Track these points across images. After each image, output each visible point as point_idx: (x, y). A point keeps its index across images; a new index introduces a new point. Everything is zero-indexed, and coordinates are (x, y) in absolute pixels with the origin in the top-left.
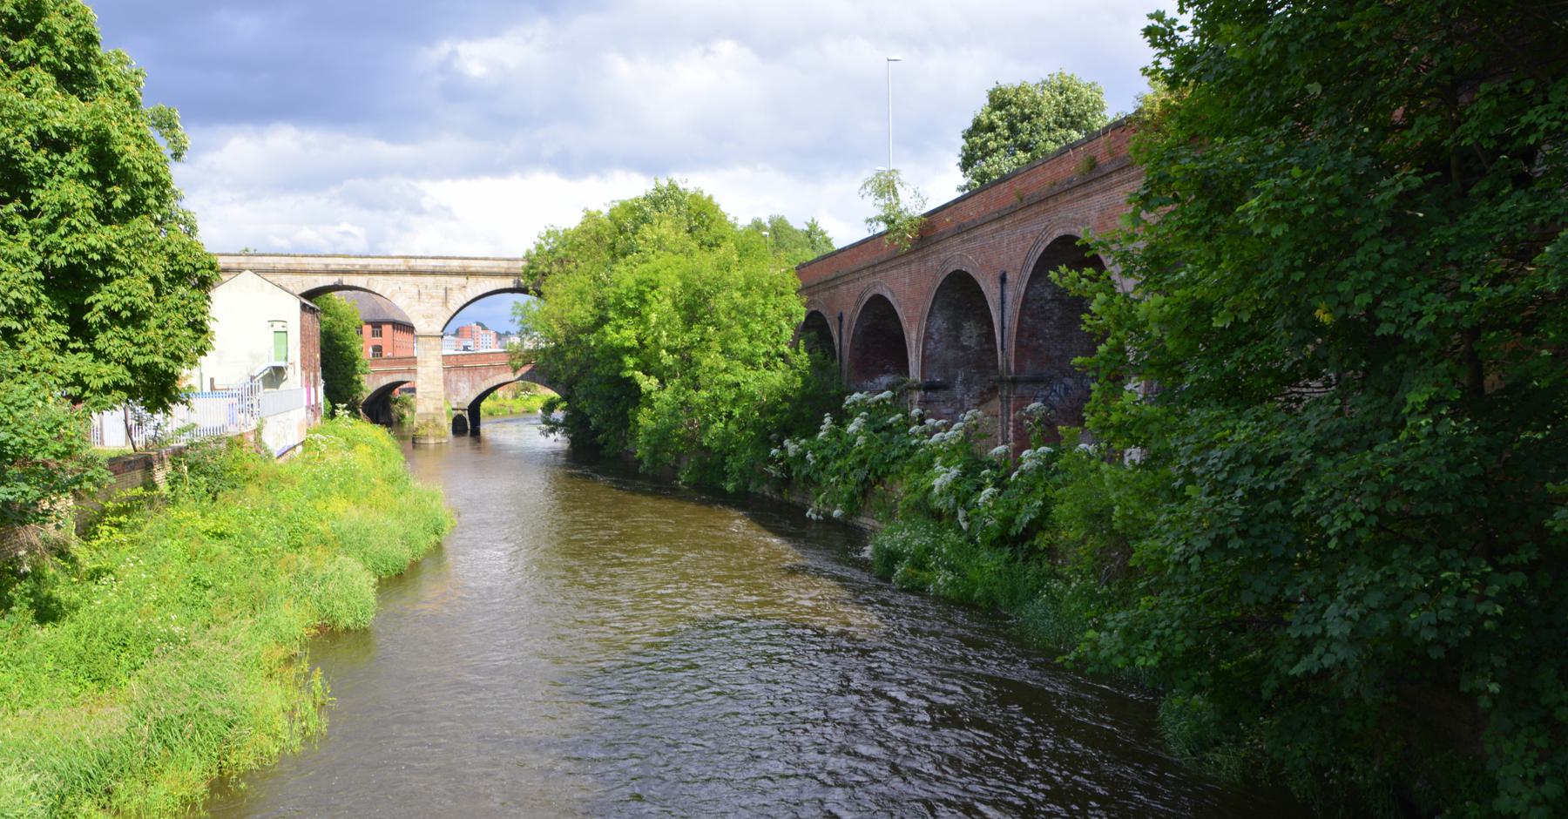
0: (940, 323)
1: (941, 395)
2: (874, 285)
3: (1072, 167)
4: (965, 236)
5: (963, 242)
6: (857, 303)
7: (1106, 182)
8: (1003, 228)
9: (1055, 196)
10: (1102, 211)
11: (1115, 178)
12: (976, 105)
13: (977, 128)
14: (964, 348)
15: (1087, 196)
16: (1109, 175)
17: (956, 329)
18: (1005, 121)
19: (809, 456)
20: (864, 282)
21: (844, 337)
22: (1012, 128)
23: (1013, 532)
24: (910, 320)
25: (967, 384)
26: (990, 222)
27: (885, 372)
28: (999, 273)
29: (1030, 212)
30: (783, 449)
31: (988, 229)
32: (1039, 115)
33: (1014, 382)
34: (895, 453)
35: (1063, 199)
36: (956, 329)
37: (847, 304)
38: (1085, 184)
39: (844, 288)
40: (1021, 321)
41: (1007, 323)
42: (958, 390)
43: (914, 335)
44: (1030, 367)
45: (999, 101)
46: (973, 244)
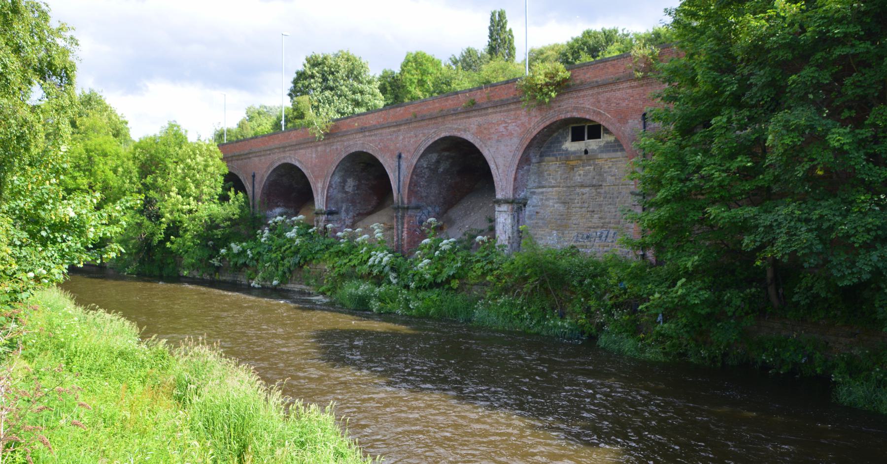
0: (337, 179)
1: (335, 217)
2: (284, 158)
3: (463, 101)
4: (367, 134)
5: (365, 136)
6: (268, 168)
7: (483, 112)
8: (399, 131)
9: (444, 116)
10: (479, 126)
11: (490, 111)
12: (300, 65)
13: (301, 76)
14: (346, 193)
15: (469, 117)
16: (487, 108)
17: (344, 182)
18: (318, 76)
19: (249, 252)
20: (276, 157)
21: (256, 186)
22: (325, 80)
23: (439, 281)
24: (316, 177)
25: (347, 211)
26: (389, 127)
27: (278, 206)
28: (397, 153)
29: (423, 123)
30: (229, 249)
31: (387, 130)
32: (338, 72)
33: (408, 208)
34: (318, 248)
35: (450, 118)
36: (344, 182)
37: (261, 169)
38: (467, 112)
39: (256, 159)
40: (411, 178)
41: (402, 179)
42: (343, 215)
43: (320, 185)
44: (414, 202)
45: (314, 63)
46: (373, 138)
